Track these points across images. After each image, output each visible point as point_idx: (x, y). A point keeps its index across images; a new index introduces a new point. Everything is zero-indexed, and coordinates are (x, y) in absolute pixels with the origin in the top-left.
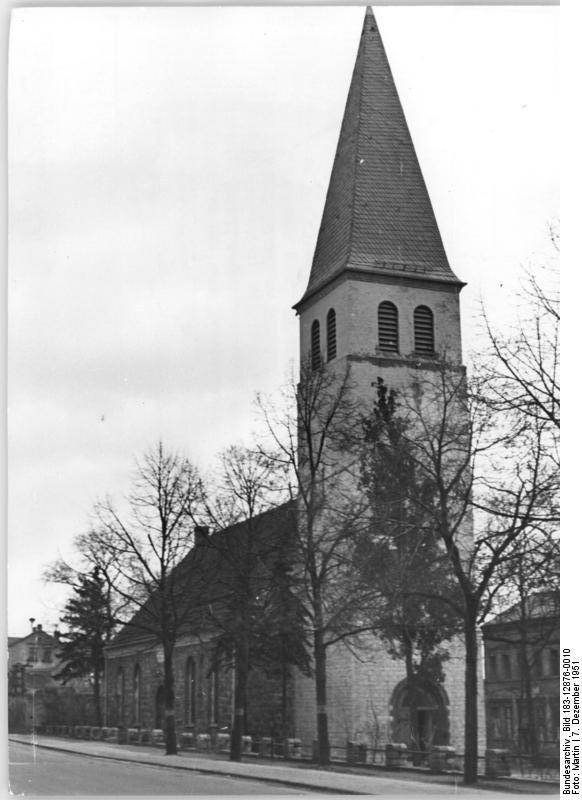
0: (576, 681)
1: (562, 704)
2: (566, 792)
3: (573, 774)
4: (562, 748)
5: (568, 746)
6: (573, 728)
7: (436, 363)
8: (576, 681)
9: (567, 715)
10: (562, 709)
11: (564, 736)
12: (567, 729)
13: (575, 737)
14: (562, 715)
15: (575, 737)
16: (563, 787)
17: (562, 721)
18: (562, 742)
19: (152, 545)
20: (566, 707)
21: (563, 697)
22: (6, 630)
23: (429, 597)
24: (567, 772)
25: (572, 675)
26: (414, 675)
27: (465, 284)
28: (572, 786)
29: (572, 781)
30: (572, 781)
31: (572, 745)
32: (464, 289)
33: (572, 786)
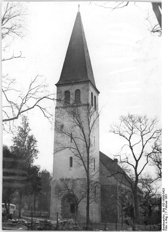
0: (166, 200)
1: (162, 204)
2: (163, 230)
3: (165, 221)
4: (162, 217)
5: (164, 216)
6: (165, 211)
7: (118, 203)
8: (166, 200)
9: (164, 207)
10: (162, 206)
11: (163, 213)
12: (164, 212)
13: (166, 213)
14: (162, 207)
15: (166, 213)
16: (162, 228)
17: (162, 209)
18: (162, 215)
19: (138, 129)
20: (164, 205)
21: (162, 202)
22: (1, 32)
23: (60, 195)
24: (164, 224)
25: (165, 198)
26: (8, 204)
27: (55, 85)
28: (165, 228)
29: (165, 226)
30: (165, 226)
31: (166, 216)
32: (56, 84)
33: (165, 228)
